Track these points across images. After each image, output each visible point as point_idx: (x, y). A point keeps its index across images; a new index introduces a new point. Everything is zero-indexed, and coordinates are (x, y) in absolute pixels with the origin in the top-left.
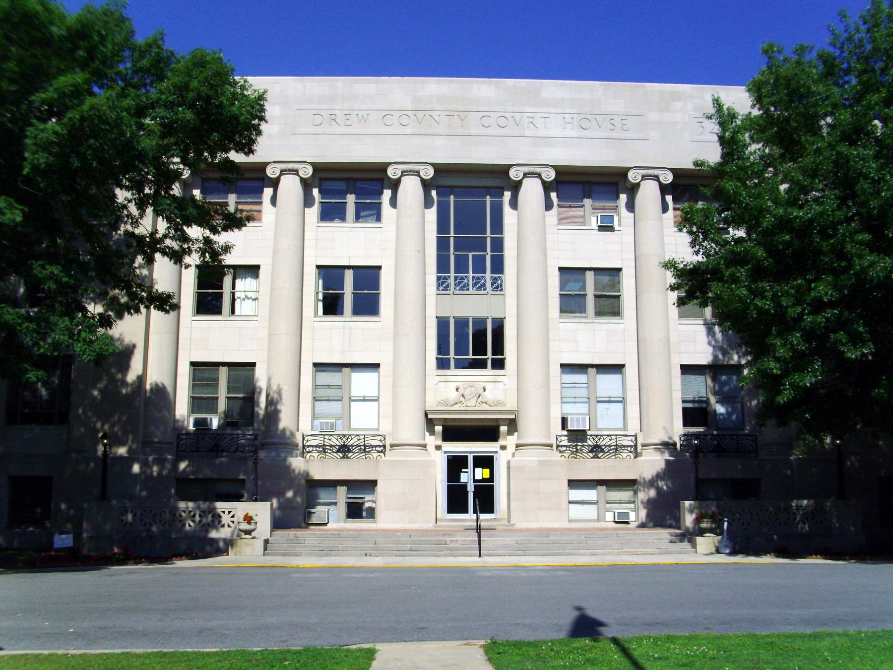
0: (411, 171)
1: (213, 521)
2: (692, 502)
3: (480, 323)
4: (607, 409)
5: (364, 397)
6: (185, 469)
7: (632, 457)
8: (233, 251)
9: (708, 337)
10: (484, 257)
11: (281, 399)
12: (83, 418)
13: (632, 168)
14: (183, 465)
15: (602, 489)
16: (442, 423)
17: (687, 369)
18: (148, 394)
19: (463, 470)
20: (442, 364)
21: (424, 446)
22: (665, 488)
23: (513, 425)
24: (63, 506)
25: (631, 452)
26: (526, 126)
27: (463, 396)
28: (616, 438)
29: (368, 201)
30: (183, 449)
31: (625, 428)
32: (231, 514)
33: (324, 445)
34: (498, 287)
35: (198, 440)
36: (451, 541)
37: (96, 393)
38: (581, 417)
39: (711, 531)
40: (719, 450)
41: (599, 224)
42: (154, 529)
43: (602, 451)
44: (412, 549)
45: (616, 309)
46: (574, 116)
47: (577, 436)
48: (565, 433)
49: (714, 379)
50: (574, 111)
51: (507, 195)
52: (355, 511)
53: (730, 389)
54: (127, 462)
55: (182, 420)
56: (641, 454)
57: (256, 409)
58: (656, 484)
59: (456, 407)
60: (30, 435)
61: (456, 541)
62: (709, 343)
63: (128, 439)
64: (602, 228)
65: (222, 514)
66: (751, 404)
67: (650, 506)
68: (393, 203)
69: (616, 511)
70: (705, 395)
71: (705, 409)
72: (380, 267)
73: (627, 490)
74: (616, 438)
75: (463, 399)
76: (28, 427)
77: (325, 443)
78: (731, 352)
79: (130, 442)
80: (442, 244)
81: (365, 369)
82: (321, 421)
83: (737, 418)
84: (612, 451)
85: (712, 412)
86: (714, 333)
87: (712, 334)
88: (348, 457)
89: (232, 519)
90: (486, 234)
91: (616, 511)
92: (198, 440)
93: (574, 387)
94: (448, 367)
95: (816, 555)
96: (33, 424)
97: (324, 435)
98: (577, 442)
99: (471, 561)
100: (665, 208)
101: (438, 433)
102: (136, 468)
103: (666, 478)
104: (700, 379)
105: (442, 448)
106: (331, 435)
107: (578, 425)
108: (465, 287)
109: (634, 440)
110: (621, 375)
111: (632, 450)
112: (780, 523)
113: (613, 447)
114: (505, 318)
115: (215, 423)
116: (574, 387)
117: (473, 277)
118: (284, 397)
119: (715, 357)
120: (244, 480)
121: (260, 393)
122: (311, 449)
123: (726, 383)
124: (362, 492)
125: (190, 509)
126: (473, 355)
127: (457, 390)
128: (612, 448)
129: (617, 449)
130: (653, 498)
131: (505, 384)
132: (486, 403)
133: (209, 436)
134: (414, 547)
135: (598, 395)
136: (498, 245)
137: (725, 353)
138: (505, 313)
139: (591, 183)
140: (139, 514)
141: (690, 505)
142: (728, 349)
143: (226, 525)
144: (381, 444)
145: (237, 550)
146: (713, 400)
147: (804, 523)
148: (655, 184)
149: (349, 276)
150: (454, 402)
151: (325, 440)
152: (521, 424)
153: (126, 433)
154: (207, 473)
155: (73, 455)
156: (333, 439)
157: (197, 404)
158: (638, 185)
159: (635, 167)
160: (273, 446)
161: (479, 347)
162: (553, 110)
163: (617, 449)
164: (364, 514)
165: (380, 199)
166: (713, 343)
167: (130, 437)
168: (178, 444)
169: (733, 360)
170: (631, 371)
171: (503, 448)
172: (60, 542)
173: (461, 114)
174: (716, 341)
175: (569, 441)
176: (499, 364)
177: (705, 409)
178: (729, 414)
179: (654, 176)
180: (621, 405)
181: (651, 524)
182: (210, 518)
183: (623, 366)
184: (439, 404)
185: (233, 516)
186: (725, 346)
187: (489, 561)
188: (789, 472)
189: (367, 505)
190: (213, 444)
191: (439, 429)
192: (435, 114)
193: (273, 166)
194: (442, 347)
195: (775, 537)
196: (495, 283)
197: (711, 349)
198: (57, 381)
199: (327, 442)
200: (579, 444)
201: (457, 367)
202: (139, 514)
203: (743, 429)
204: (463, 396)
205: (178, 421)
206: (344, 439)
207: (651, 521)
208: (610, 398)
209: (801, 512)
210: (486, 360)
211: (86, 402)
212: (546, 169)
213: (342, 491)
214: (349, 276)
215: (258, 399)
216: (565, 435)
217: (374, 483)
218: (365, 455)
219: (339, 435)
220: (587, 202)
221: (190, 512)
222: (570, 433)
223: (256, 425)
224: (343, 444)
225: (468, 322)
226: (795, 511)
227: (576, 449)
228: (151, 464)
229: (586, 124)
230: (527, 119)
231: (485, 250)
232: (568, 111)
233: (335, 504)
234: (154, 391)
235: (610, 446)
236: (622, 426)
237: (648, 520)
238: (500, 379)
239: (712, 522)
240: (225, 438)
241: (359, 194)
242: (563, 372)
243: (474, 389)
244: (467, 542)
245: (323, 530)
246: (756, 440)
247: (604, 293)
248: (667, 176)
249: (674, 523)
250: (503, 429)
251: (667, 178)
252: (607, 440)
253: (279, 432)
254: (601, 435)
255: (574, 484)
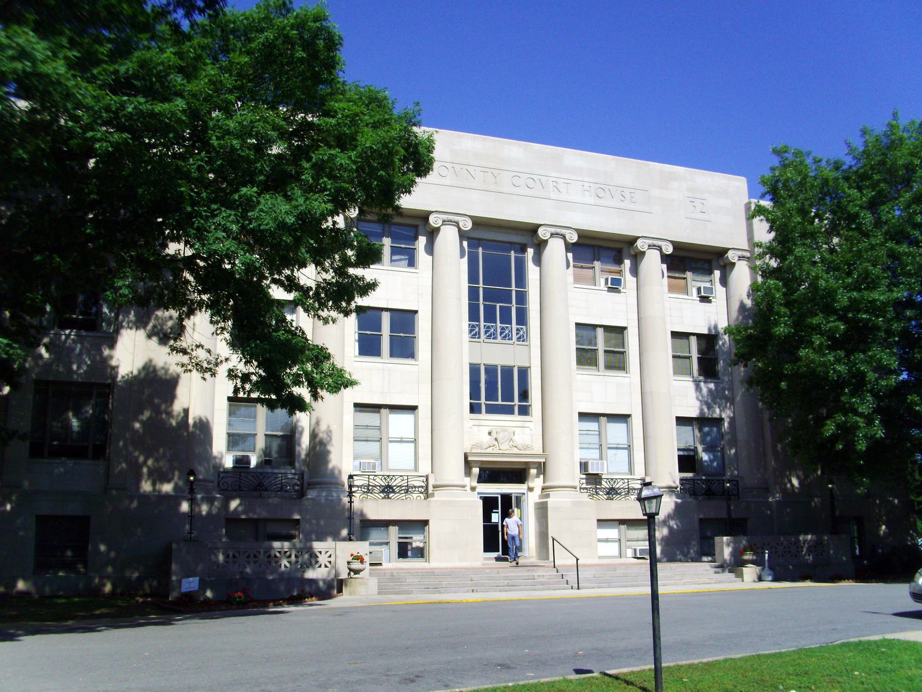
0: (451, 221)
1: (310, 559)
2: (729, 537)
3: (507, 372)
4: (615, 455)
5: (402, 438)
6: (236, 509)
7: (423, 498)
8: (378, 289)
9: (696, 393)
10: (510, 309)
11: (331, 439)
12: (124, 452)
13: (433, 212)
14: (234, 504)
15: (623, 527)
16: (479, 465)
17: (681, 421)
18: (191, 429)
19: (494, 511)
20: (474, 409)
21: (464, 486)
22: (675, 527)
23: (542, 468)
24: (103, 548)
25: (421, 493)
26: (552, 190)
27: (496, 439)
28: (628, 482)
29: (403, 246)
30: (225, 488)
31: (416, 469)
32: (328, 554)
33: (369, 485)
34: (523, 338)
35: (240, 479)
36: (539, 576)
37: (137, 425)
38: (595, 461)
39: (753, 562)
40: (709, 494)
41: (610, 286)
42: (248, 570)
43: (394, 492)
44: (509, 584)
45: (622, 366)
46: (591, 184)
47: (240, 473)
48: (584, 476)
49: (700, 430)
50: (592, 180)
51: (530, 252)
52: (403, 551)
53: (711, 439)
54: (173, 500)
55: (220, 456)
56: (433, 495)
57: (297, 448)
58: (668, 524)
59: (490, 450)
60: (62, 470)
61: (543, 576)
62: (697, 398)
63: (173, 474)
64: (610, 290)
65: (318, 554)
66: (730, 452)
67: (663, 543)
68: (430, 249)
69: (638, 548)
70: (693, 444)
71: (693, 457)
72: (416, 312)
73: (642, 529)
74: (628, 482)
75: (496, 443)
76: (58, 461)
77: (370, 484)
78: (714, 406)
79: (176, 478)
80: (473, 294)
81: (401, 410)
82: (362, 461)
83: (717, 465)
84: (403, 492)
85: (699, 458)
86: (701, 389)
87: (699, 390)
88: (389, 498)
89: (330, 559)
90: (479, 284)
91: (638, 548)
92: (240, 479)
93: (587, 434)
94: (480, 412)
95: (848, 580)
96: (63, 458)
97: (369, 475)
98: (596, 485)
99: (575, 593)
100: (568, 266)
101: (475, 475)
102: (185, 507)
103: (676, 518)
104: (688, 429)
105: (477, 489)
106: (376, 476)
107: (598, 469)
108: (492, 336)
109: (425, 480)
110: (626, 425)
111: (423, 490)
112: (792, 556)
113: (404, 488)
114: (530, 367)
115: (254, 462)
116: (587, 434)
117: (485, 326)
118: (334, 437)
119: (702, 410)
120: (299, 520)
121: (301, 433)
122: (356, 489)
123: (708, 434)
124: (411, 531)
125: (286, 550)
126: (502, 401)
127: (490, 434)
128: (403, 488)
129: (408, 490)
130: (666, 537)
131: (531, 430)
132: (516, 447)
133: (252, 474)
134: (511, 583)
135: (609, 442)
136: (522, 298)
137: (709, 407)
138: (530, 363)
139: (600, 247)
140: (231, 555)
141: (727, 540)
142: (712, 403)
143: (323, 566)
144: (423, 485)
145: (352, 590)
146: (700, 448)
147: (809, 555)
148: (657, 253)
149: (386, 318)
150: (488, 446)
151: (370, 480)
152: (550, 469)
153: (172, 469)
154: (261, 513)
155: (114, 492)
156: (378, 480)
157: (234, 440)
158: (438, 229)
159: (436, 211)
160: (324, 486)
161: (508, 396)
162: (574, 177)
163: (408, 490)
164: (409, 553)
165: (414, 245)
166: (700, 398)
167: (176, 473)
168: (219, 484)
169: (716, 413)
170: (424, 412)
171: (530, 489)
172: (187, 585)
173: (493, 171)
174: (702, 397)
175: (587, 483)
176: (524, 411)
177: (693, 457)
178: (711, 461)
179: (658, 247)
180: (378, 443)
181: (665, 559)
182: (306, 556)
183: (629, 416)
184: (473, 446)
185: (330, 556)
186: (710, 401)
187: (583, 593)
188: (769, 512)
189: (414, 545)
190: (257, 483)
191: (476, 471)
192: (471, 169)
193: (437, 215)
194: (474, 393)
195: (791, 567)
196: (504, 332)
197: (698, 404)
198: (91, 411)
199: (372, 483)
200: (598, 486)
201: (488, 412)
202: (231, 555)
203: (724, 475)
204: (496, 439)
205: (215, 458)
206: (388, 480)
207: (665, 556)
208: (619, 444)
209: (806, 545)
210: (513, 406)
211: (127, 435)
212: (569, 231)
213: (394, 530)
214: (386, 318)
215: (300, 439)
216: (583, 479)
217: (425, 523)
218: (405, 496)
219: (608, 479)
220: (597, 264)
221: (286, 552)
222: (588, 476)
223: (297, 465)
224: (387, 484)
225: (497, 370)
226: (802, 544)
227: (368, 489)
228: (199, 502)
229: (601, 194)
230: (552, 183)
231: (511, 303)
232: (586, 179)
233: (387, 543)
234: (198, 425)
235: (401, 486)
236: (413, 468)
237: (663, 556)
238: (527, 424)
239: (754, 554)
240: (269, 477)
241: (395, 238)
242: (580, 420)
243: (506, 433)
244: (552, 577)
245: (380, 570)
246: (738, 484)
247: (612, 349)
248: (466, 223)
249: (683, 558)
250: (533, 471)
251: (668, 250)
252: (399, 480)
253: (329, 471)
254: (616, 479)
255: (602, 523)
